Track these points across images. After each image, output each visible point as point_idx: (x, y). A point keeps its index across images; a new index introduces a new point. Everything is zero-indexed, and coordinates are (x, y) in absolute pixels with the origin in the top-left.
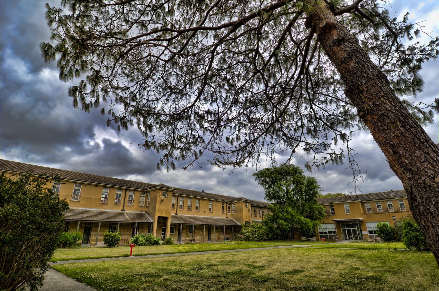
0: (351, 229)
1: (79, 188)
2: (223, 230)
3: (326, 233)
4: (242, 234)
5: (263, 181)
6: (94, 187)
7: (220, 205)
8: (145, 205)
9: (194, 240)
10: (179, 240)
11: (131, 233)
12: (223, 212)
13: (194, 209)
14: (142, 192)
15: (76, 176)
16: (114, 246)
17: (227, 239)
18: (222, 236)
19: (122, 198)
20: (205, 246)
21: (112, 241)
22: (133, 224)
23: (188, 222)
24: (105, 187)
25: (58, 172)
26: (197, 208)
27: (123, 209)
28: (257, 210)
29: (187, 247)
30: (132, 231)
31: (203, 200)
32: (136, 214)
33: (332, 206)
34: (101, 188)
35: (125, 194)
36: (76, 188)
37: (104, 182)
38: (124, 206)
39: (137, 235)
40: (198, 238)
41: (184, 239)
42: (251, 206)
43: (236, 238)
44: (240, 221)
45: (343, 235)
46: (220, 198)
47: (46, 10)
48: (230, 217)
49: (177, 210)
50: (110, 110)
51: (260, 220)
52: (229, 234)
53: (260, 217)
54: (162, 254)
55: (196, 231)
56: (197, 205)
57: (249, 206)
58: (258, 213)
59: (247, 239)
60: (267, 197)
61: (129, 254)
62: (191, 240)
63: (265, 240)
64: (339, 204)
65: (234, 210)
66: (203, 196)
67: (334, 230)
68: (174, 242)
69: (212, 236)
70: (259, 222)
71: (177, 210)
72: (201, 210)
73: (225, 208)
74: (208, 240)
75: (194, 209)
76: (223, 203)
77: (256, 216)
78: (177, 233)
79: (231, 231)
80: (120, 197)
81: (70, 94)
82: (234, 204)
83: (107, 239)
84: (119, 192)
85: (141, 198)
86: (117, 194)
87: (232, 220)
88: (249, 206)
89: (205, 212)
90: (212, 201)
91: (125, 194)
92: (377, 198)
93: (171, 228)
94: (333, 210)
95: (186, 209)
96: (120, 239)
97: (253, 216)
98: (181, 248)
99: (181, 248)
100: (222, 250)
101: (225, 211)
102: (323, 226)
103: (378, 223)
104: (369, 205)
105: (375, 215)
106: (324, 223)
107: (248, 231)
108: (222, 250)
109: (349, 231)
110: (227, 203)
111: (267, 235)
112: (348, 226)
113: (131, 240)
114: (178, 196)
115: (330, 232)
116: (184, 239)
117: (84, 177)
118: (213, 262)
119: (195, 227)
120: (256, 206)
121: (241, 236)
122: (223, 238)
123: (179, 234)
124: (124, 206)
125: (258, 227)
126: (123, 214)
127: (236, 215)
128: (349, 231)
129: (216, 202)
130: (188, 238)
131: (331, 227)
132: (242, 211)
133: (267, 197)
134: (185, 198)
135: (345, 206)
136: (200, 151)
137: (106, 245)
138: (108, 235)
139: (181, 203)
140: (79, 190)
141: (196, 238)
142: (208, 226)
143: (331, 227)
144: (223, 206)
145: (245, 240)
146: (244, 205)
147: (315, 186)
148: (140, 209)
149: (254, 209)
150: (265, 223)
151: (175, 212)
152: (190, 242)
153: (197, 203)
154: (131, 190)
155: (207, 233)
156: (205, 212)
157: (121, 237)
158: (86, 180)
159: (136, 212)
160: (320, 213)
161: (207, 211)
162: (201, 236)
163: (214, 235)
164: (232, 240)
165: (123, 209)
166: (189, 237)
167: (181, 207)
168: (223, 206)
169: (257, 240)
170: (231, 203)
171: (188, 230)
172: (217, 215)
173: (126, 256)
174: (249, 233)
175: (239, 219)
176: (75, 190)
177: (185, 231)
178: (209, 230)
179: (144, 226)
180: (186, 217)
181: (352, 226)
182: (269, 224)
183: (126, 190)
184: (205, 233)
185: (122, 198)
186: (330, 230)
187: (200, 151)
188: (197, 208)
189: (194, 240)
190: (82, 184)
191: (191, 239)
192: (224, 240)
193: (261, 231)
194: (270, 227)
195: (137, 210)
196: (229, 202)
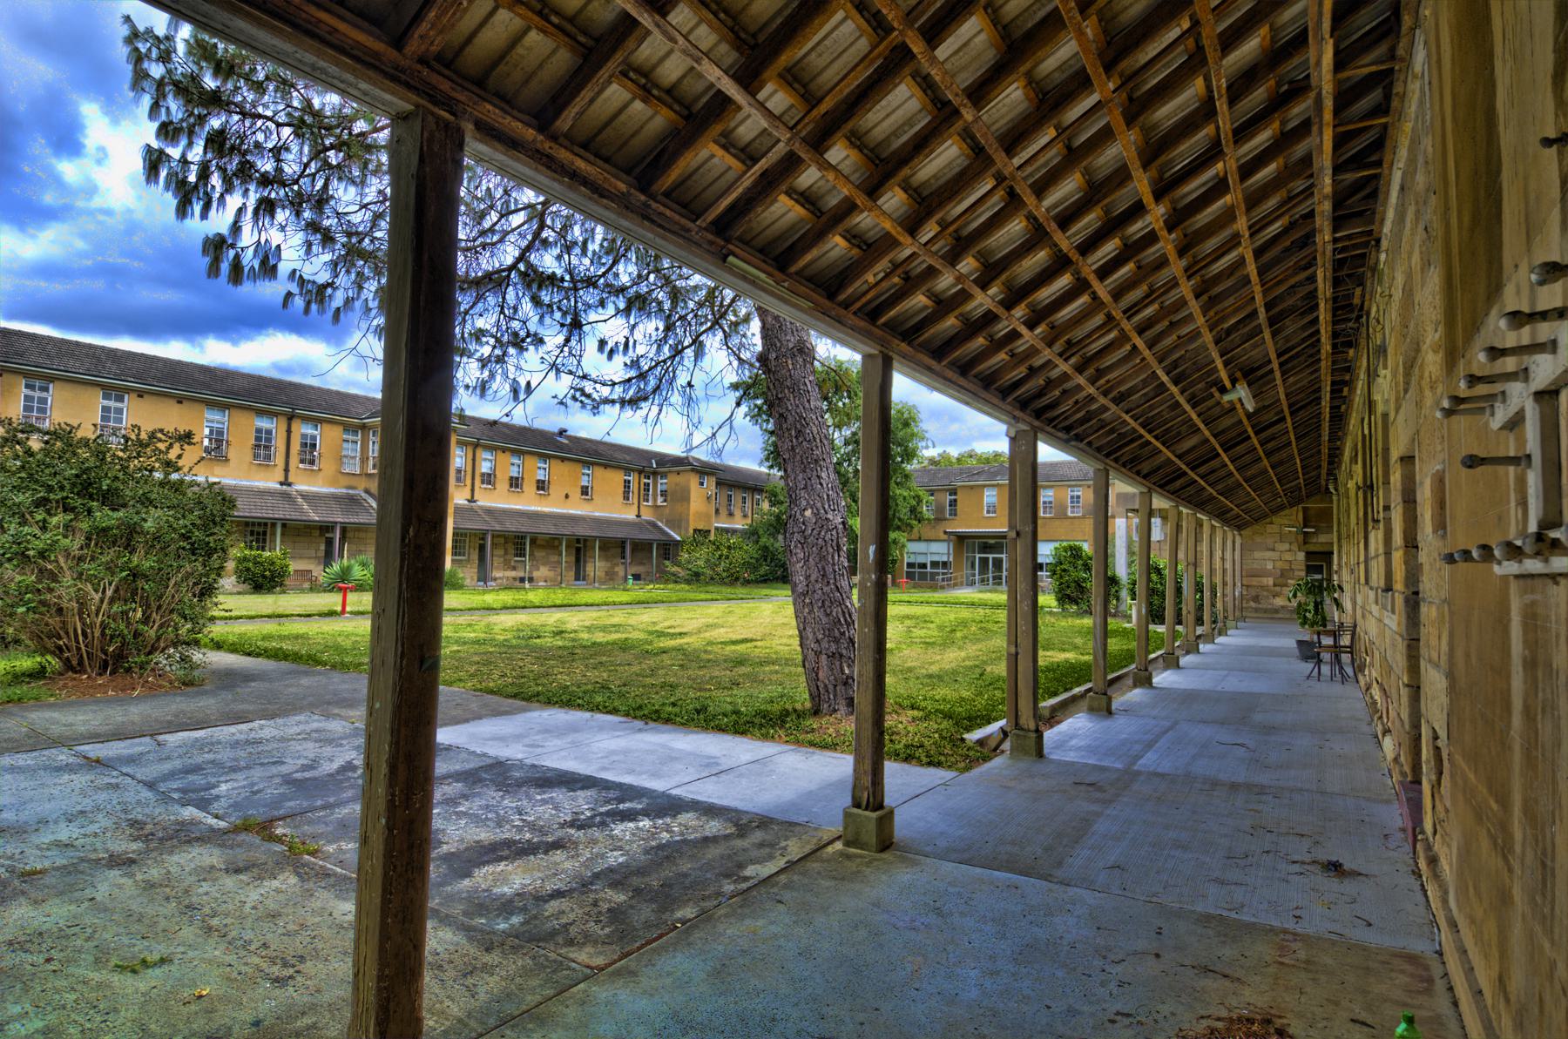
0: (991, 556)
1: (119, 405)
2: (623, 552)
3: (924, 566)
4: (679, 564)
5: (760, 408)
6: (173, 402)
7: (618, 478)
8: (362, 468)
9: (531, 580)
10: (483, 577)
11: (322, 554)
12: (626, 498)
13: (529, 487)
14: (348, 428)
15: (99, 360)
16: (270, 590)
17: (637, 577)
18: (620, 570)
19: (279, 443)
20: (559, 596)
21: (264, 577)
22: (325, 529)
23: (511, 526)
24: (211, 405)
25: (28, 343)
26: (541, 485)
27: (286, 477)
28: (737, 496)
29: (507, 597)
30: (323, 547)
31: (563, 459)
32: (334, 497)
33: (954, 492)
34: (197, 406)
35: (289, 432)
36: (106, 403)
37: (208, 387)
38: (286, 470)
39: (345, 560)
40: (543, 572)
41: (497, 574)
42: (718, 484)
43: (663, 577)
44: (680, 527)
45: (967, 571)
46: (618, 455)
47: (125, 31)
48: (647, 515)
49: (473, 490)
50: (294, 271)
51: (739, 524)
52: (642, 564)
53: (745, 516)
54: (857, 65)
55: (539, 554)
56: (541, 475)
57: (710, 483)
58: (740, 504)
59: (695, 578)
60: (767, 459)
61: (339, 609)
62: (522, 580)
63: (747, 582)
64: (972, 487)
65: (664, 493)
66: (561, 448)
67: (945, 559)
68: (467, 582)
69: (589, 568)
70: (734, 531)
71: (473, 490)
72: (556, 491)
73: (634, 486)
74: (577, 578)
75: (529, 487)
76: (628, 471)
77: (731, 514)
78: (475, 556)
79: (645, 554)
80: (269, 440)
81: (205, 251)
82: (664, 476)
83: (248, 570)
84: (264, 423)
85: (345, 445)
86: (259, 431)
87: (654, 525)
88: (710, 483)
89: (567, 496)
90: (593, 464)
91: (289, 432)
92: (1074, 476)
93: (455, 541)
94: (953, 503)
95: (502, 485)
96: (291, 569)
97: (723, 512)
98: (490, 599)
99: (490, 599)
100: (606, 604)
101: (634, 498)
102: (912, 547)
103: (1057, 545)
104: (1050, 493)
105: (1057, 522)
106: (920, 539)
107: (699, 558)
108: (606, 604)
109: (984, 562)
110: (640, 472)
111: (755, 569)
112: (986, 548)
113: (320, 574)
114: (476, 446)
115: (935, 564)
116: (497, 574)
117: (129, 364)
118: (569, 627)
119: (533, 541)
120: (731, 483)
121: (675, 569)
122: (622, 573)
123: (482, 558)
124: (286, 470)
125: (729, 548)
126: (287, 497)
127: (667, 511)
128: (984, 562)
129: (606, 466)
130: (513, 574)
131: (940, 550)
132: (684, 497)
133: (767, 459)
134: (499, 453)
135: (987, 492)
136: (528, 383)
137: (246, 587)
138: (245, 559)
139: (485, 467)
140: (119, 411)
141: (535, 574)
142: (578, 541)
143: (940, 550)
144: (627, 482)
145: (688, 582)
146: (693, 480)
147: (913, 435)
148: (345, 481)
149: (725, 492)
150: (752, 534)
151: (466, 493)
152: (517, 584)
153: (537, 470)
154: (306, 419)
155: (573, 559)
156: (567, 496)
157: (293, 566)
158: (139, 378)
159: (332, 490)
160: (913, 510)
161: (576, 494)
162: (553, 568)
163: (596, 566)
164: (651, 582)
165: (286, 477)
166: (514, 568)
167: (489, 479)
168: (627, 482)
169: (722, 582)
170: (655, 473)
171: (512, 551)
172: (610, 505)
173: (331, 614)
174: (701, 563)
175: (676, 523)
176: (106, 409)
177: (501, 552)
178: (578, 550)
179: (362, 535)
180: (505, 512)
181: (996, 548)
182: (763, 540)
183: (291, 418)
184: (566, 558)
185: (279, 443)
186: (936, 558)
187: (528, 383)
188: (541, 485)
189: (531, 580)
190: (129, 390)
191: (521, 574)
192: (626, 579)
193: (737, 556)
194: (765, 548)
195: (334, 483)
196: (646, 467)
